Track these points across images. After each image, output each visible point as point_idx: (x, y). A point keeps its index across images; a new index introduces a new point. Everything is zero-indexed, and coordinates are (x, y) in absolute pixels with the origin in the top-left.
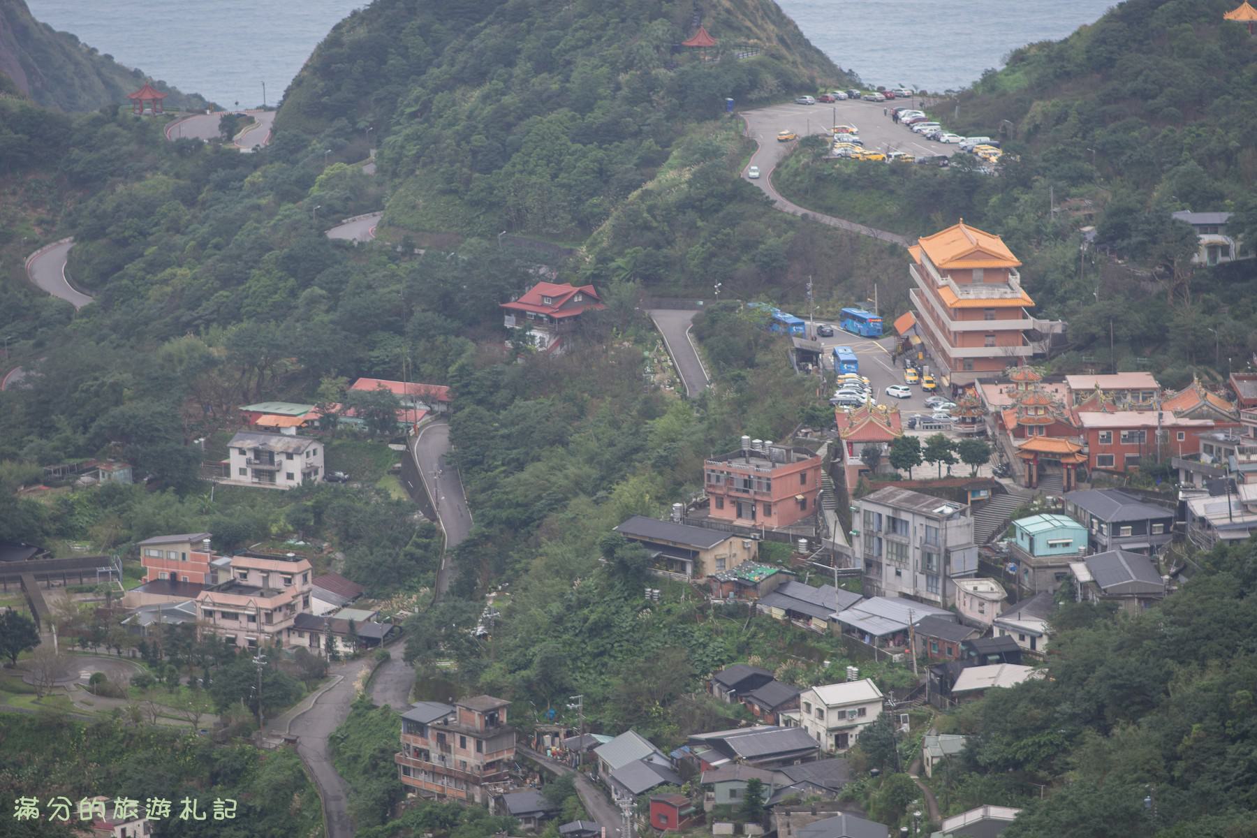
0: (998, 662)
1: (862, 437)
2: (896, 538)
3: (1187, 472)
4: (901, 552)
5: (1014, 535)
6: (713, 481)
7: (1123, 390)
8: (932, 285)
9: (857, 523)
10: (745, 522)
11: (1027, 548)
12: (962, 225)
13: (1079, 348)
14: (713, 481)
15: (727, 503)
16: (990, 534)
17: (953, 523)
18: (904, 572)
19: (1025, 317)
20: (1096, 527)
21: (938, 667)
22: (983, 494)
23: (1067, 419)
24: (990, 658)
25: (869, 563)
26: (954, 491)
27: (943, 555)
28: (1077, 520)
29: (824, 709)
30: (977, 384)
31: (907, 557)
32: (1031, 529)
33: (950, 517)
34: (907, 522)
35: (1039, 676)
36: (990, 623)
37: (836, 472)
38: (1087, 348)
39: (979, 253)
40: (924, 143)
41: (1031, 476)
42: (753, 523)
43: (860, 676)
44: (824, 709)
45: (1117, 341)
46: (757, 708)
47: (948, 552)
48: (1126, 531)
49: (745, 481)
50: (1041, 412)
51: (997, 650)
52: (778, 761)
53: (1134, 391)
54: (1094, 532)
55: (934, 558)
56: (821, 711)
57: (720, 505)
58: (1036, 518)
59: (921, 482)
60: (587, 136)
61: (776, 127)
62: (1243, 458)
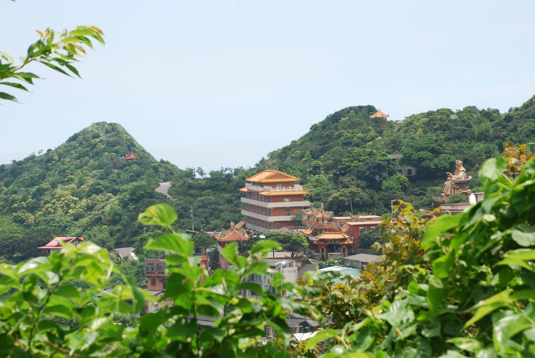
6: (150, 270)
15: (157, 282)
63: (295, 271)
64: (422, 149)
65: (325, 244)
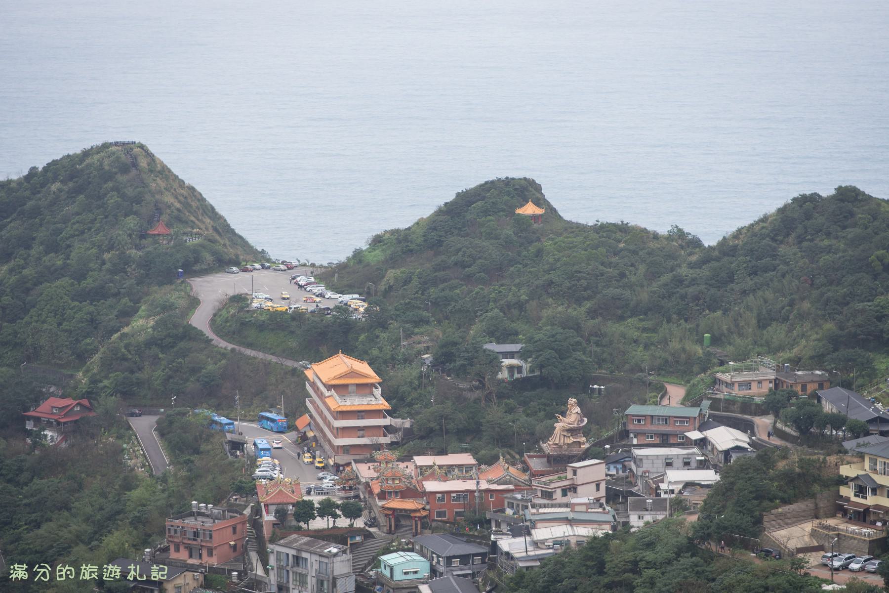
1: (274, 501)
2: (299, 570)
3: (496, 521)
5: (379, 567)
6: (172, 533)
8: (321, 396)
9: (272, 561)
10: (194, 561)
11: (388, 575)
12: (341, 355)
13: (422, 438)
14: (172, 533)
15: (182, 548)
16: (363, 565)
17: (338, 559)
19: (385, 417)
20: (435, 560)
28: (423, 555)
30: (353, 463)
32: (391, 562)
33: (335, 555)
34: (306, 559)
37: (257, 525)
39: (353, 373)
41: (390, 526)
45: (447, 432)
47: (334, 579)
48: (456, 562)
49: (194, 533)
50: (397, 482)
53: (460, 467)
55: (325, 583)
57: (177, 550)
58: (394, 555)
60: (82, 296)
62: (534, 511)
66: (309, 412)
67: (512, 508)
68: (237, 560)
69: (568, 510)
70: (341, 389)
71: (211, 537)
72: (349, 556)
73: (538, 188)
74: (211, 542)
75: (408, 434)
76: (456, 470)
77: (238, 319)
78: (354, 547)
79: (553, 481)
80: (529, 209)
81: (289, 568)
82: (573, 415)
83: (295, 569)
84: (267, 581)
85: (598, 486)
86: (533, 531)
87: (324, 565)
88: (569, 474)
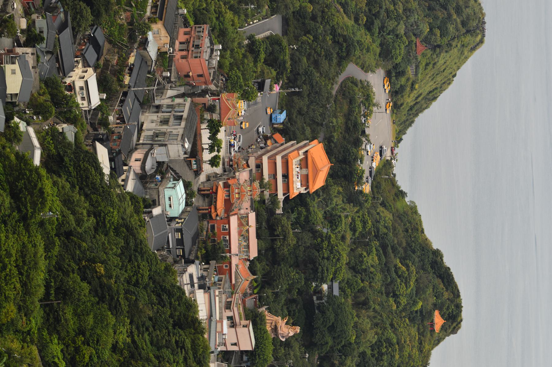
0: (111, 168)
1: (222, 104)
2: (172, 120)
3: (208, 268)
4: (165, 122)
5: (174, 180)
6: (198, 29)
7: (249, 241)
8: (299, 149)
9: (178, 101)
10: (177, 45)
11: (169, 186)
12: (330, 165)
13: (268, 221)
14: (198, 29)
17: (180, 148)
18: (154, 124)
19: (284, 194)
20: (179, 221)
21: (107, 137)
22: (195, 167)
23: (233, 210)
24: (113, 163)
25: (158, 107)
26: (195, 153)
27: (164, 143)
28: (183, 212)
29: (85, 79)
30: (249, 169)
31: (161, 125)
32: (178, 187)
33: (183, 146)
34: (180, 125)
35: (106, 178)
36: (130, 165)
37: (204, 93)
38: (268, 226)
39: (316, 172)
40: (369, 162)
41: (204, 190)
42: (177, 50)
43: (101, 100)
44: (85, 79)
45: (273, 241)
46: (83, 47)
50: (237, 196)
51: (117, 167)
52: (57, 55)
53: (248, 247)
54: (177, 220)
56: (83, 78)
58: (183, 191)
59: (200, 134)
61: (377, 83)
62: (217, 293)
63: (179, 156)
64: (337, 315)
65: (214, 193)
66: (286, 143)
67: (219, 281)
68: (179, 78)
69: (218, 319)
70: (304, 163)
71: (196, 57)
72: (183, 156)
73: (454, 331)
74: (192, 57)
75: (271, 212)
76: (245, 244)
77: (355, 99)
78: (189, 164)
79: (238, 309)
80: (438, 321)
81: (173, 113)
82: (287, 331)
83: (172, 117)
84: (163, 97)
85: (235, 344)
86: (202, 291)
87: (176, 138)
88: (244, 322)
